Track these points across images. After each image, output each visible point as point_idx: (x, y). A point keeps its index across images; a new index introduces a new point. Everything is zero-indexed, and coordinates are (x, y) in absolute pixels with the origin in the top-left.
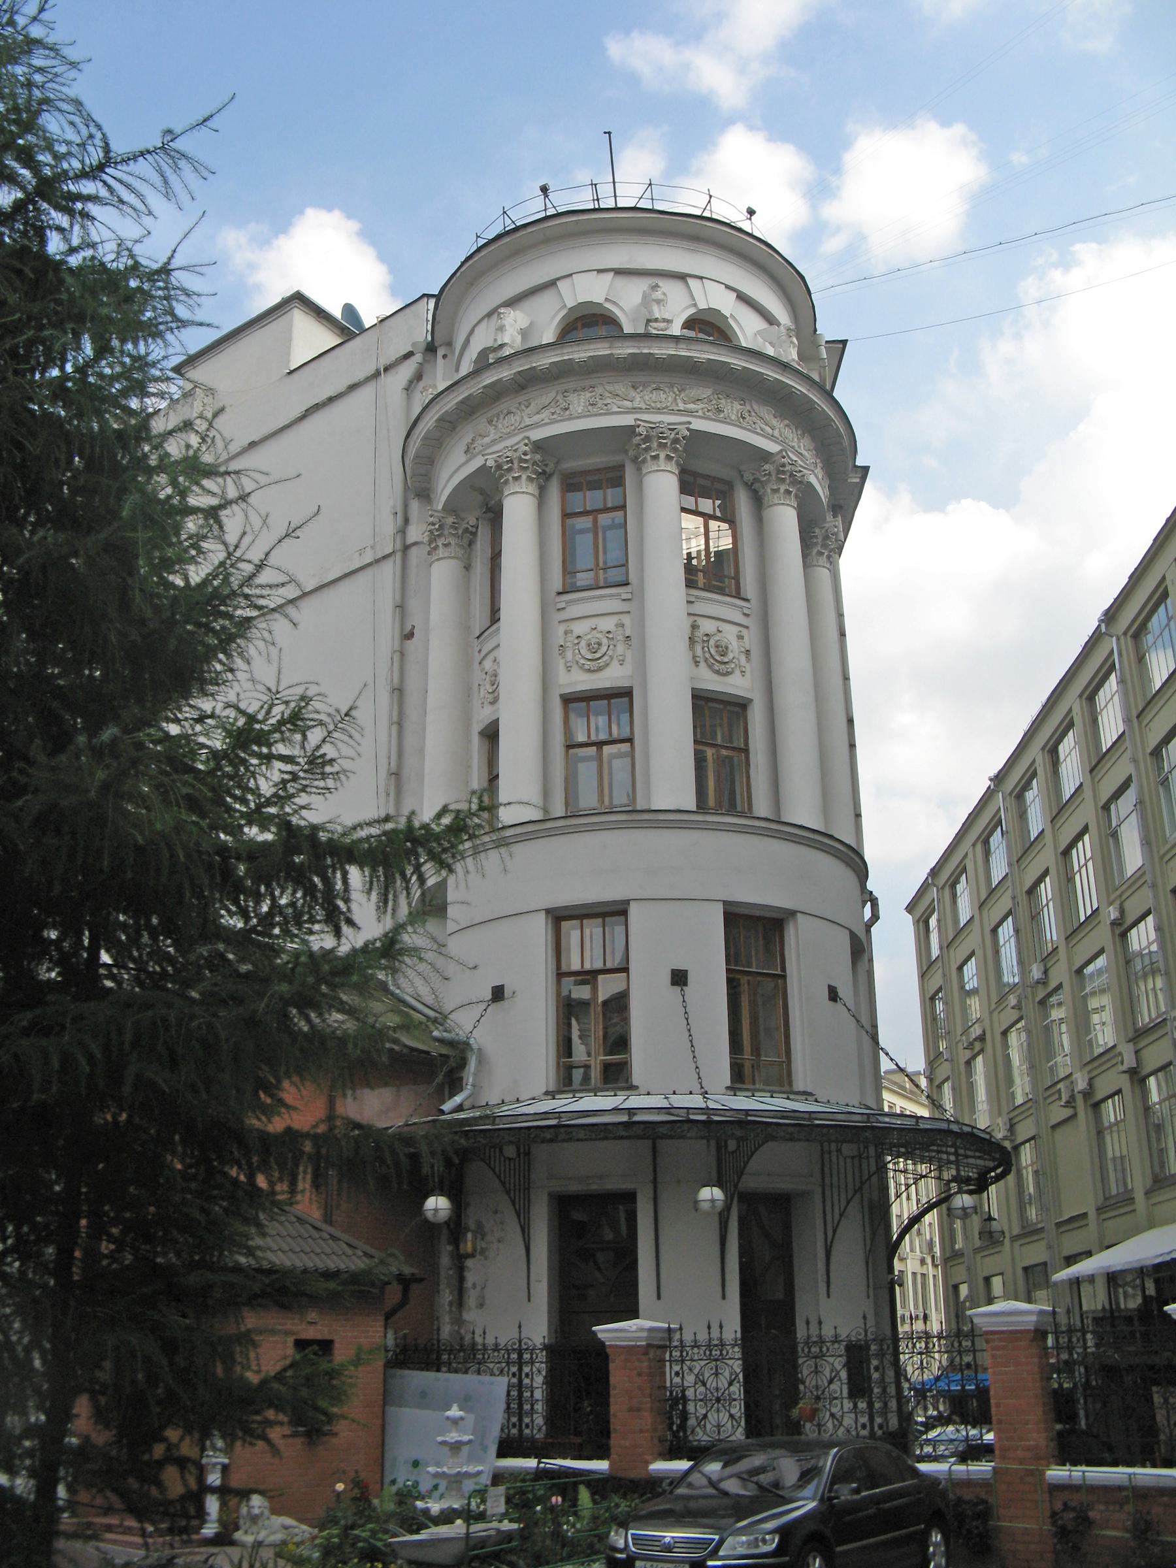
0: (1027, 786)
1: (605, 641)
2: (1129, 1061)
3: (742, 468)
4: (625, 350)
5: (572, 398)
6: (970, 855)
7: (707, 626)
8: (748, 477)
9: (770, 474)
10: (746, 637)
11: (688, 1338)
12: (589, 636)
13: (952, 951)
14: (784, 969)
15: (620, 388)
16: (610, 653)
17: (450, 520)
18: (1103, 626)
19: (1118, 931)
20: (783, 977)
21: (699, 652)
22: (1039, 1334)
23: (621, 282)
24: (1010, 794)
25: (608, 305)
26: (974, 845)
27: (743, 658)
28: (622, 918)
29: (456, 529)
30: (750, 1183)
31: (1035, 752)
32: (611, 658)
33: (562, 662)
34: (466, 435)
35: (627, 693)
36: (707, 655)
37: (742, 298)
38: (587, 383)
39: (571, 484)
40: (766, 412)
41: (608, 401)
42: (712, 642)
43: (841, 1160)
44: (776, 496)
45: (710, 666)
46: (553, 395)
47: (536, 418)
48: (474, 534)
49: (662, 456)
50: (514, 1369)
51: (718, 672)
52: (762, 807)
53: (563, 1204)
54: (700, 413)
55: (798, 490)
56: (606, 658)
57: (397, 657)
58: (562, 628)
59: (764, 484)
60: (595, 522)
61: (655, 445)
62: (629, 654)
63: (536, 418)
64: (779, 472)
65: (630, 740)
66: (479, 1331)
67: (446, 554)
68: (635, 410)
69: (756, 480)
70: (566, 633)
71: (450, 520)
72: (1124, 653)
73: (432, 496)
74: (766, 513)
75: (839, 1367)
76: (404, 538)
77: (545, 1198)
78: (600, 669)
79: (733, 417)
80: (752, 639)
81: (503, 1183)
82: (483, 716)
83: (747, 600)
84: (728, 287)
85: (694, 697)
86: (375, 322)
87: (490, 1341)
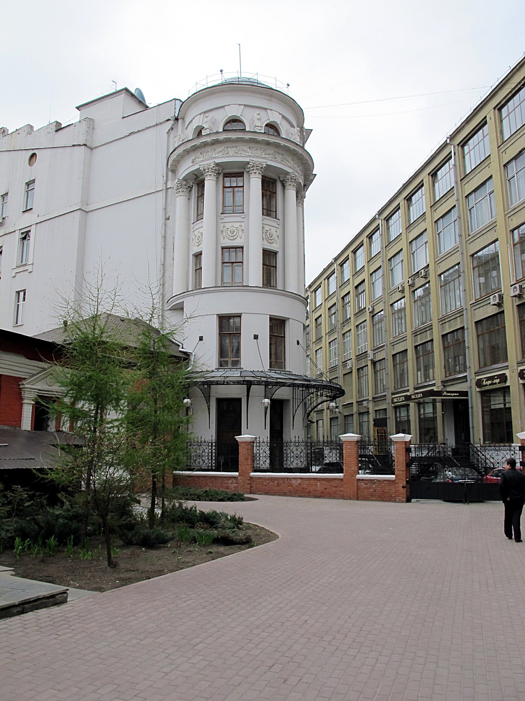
0: (344, 262)
1: (236, 231)
2: (371, 357)
3: (280, 176)
4: (247, 136)
5: (230, 149)
6: (323, 282)
7: (267, 228)
8: (282, 179)
9: (288, 179)
10: (278, 232)
11: (261, 441)
12: (231, 229)
13: (314, 313)
14: (284, 335)
15: (245, 148)
16: (237, 234)
17: (184, 183)
18: (377, 216)
19: (372, 315)
20: (284, 337)
21: (264, 236)
22: (357, 442)
23: (247, 109)
24: (339, 264)
25: (241, 117)
26: (325, 279)
27: (277, 238)
28: (239, 318)
29: (186, 186)
30: (275, 397)
31: (349, 252)
32: (238, 236)
33: (222, 236)
34: (192, 156)
35: (242, 248)
36: (266, 237)
37: (283, 117)
38: (236, 145)
39: (226, 175)
40: (289, 158)
41: (241, 152)
42: (268, 233)
43: (299, 391)
44: (290, 186)
45: (267, 241)
46: (223, 148)
47: (217, 155)
48: (192, 188)
49: (257, 172)
50: (210, 448)
51: (269, 243)
52: (280, 286)
53: (219, 401)
54: (269, 159)
55: (297, 185)
56: (236, 236)
57: (163, 226)
58: (222, 225)
59: (286, 182)
60: (234, 190)
61: (255, 168)
62: (243, 235)
63: (217, 155)
64: (291, 179)
65: (242, 262)
66: (200, 438)
67: (183, 194)
68: (250, 156)
69: (284, 180)
70: (223, 227)
71: (184, 183)
72: (383, 225)
73: (176, 172)
74: (286, 191)
75: (303, 449)
76: (166, 186)
77: (215, 400)
78: (234, 239)
79: (279, 160)
80: (280, 232)
81: (204, 395)
82: (196, 250)
83: (279, 220)
84: (280, 113)
85: (263, 250)
86: (156, 105)
87: (203, 440)
